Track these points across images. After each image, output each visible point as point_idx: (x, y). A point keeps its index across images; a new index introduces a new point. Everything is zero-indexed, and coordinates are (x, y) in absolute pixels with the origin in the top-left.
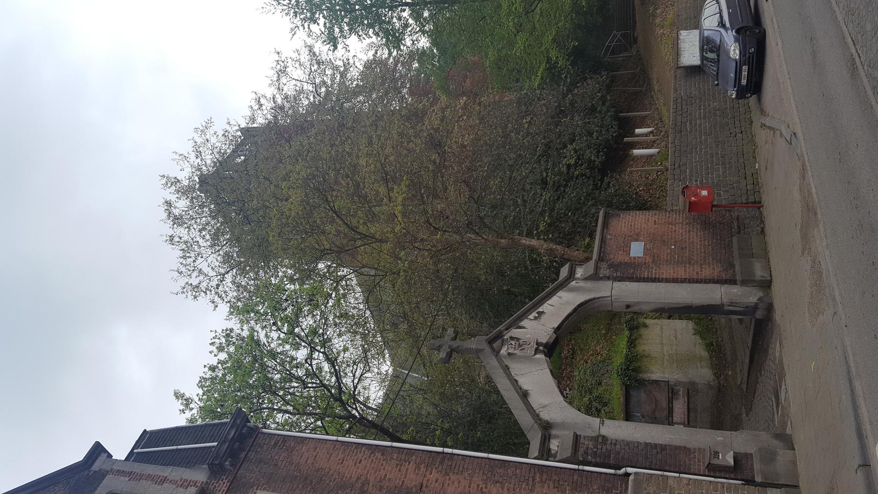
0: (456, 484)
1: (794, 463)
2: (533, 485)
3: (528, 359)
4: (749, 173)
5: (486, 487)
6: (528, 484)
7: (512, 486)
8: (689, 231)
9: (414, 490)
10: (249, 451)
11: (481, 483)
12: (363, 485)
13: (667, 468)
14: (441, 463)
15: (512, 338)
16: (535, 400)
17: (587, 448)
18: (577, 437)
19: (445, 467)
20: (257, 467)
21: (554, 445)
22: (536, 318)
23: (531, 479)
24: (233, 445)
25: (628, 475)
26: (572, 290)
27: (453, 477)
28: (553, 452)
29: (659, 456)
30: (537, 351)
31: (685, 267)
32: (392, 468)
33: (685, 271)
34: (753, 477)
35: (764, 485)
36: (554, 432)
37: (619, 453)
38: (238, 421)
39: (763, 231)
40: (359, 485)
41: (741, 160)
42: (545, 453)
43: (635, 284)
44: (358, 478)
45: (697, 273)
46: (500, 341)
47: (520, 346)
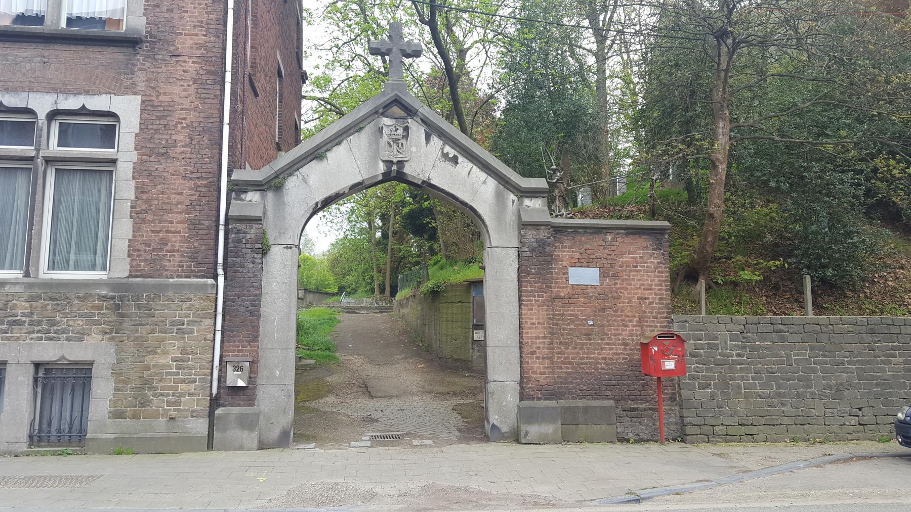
0: (184, 94)
1: (241, 448)
3: (375, 154)
4: (754, 430)
5: (183, 128)
6: (192, 172)
7: (188, 155)
11: (188, 121)
13: (227, 318)
14: (209, 72)
15: (406, 129)
16: (313, 170)
18: (258, 220)
19: (204, 77)
22: (445, 156)
23: (200, 175)
25: (215, 277)
27: (192, 89)
28: (243, 196)
29: (242, 309)
30: (389, 163)
31: (545, 338)
32: (196, 17)
34: (223, 406)
35: (211, 415)
36: (270, 195)
39: (624, 440)
41: (786, 420)
42: (238, 189)
45: (533, 353)
46: (402, 113)
47: (396, 141)
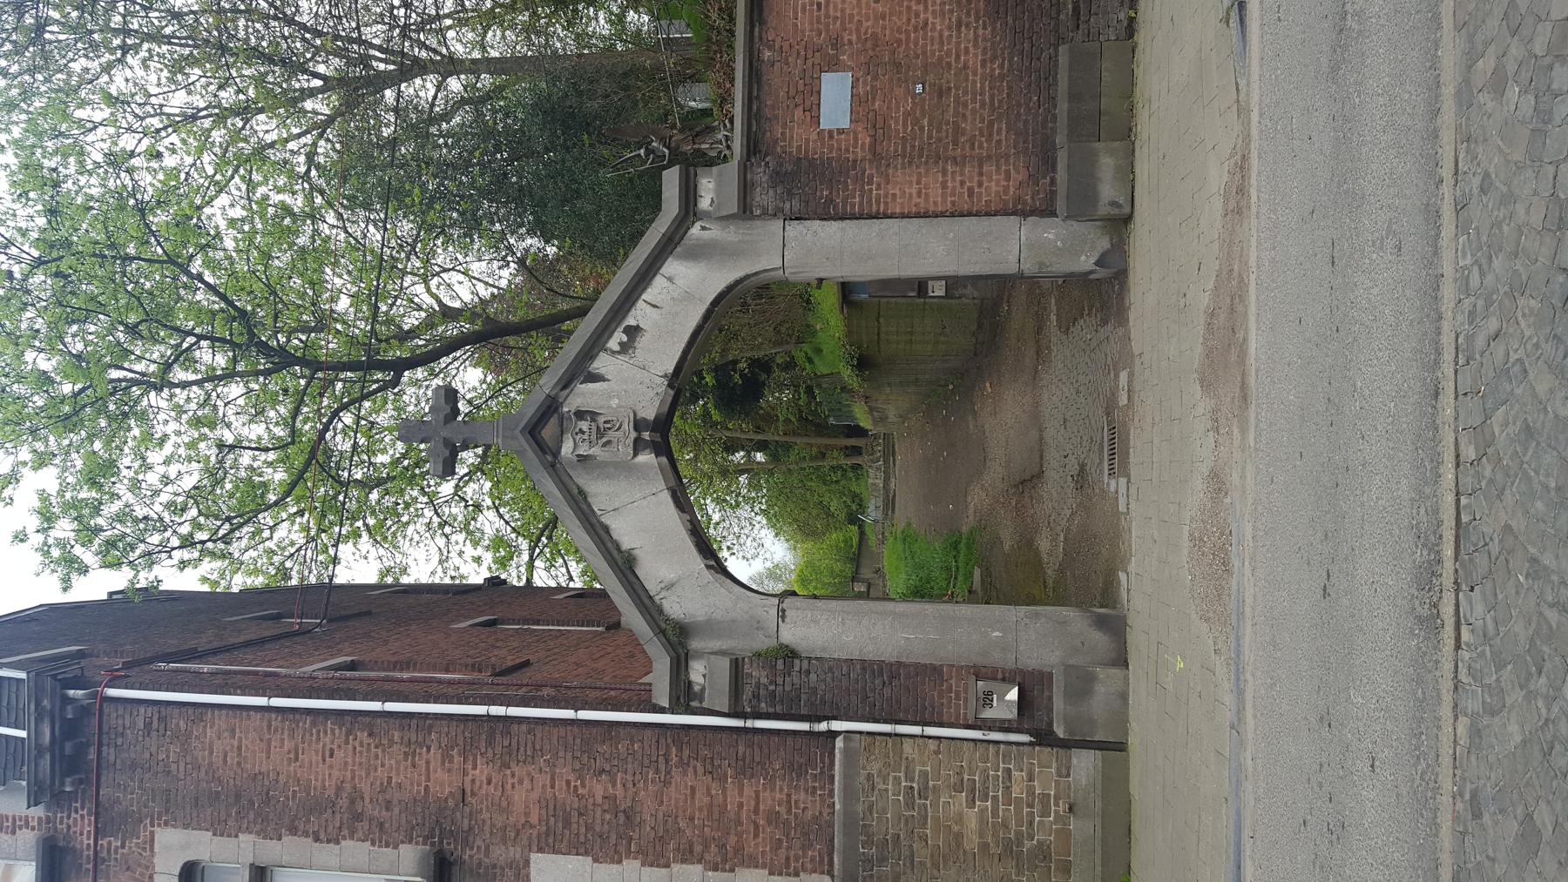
0: (526, 782)
1: (1124, 697)
2: (668, 773)
3: (625, 469)
5: (583, 786)
6: (657, 771)
7: (630, 778)
8: (959, 25)
9: (451, 803)
10: (100, 745)
11: (571, 777)
12: (352, 802)
14: (490, 742)
15: (580, 415)
16: (652, 572)
17: (758, 685)
18: (736, 665)
19: (498, 750)
20: (132, 780)
21: (697, 673)
22: (625, 348)
24: (62, 749)
25: (833, 734)
26: (699, 253)
28: (697, 688)
30: (638, 446)
32: (398, 763)
33: (944, 185)
34: (1050, 724)
37: (814, 691)
38: (46, 703)
39: (1131, 28)
40: (343, 802)
43: (834, 226)
44: (339, 789)
45: (971, 192)
46: (554, 421)
47: (600, 433)
